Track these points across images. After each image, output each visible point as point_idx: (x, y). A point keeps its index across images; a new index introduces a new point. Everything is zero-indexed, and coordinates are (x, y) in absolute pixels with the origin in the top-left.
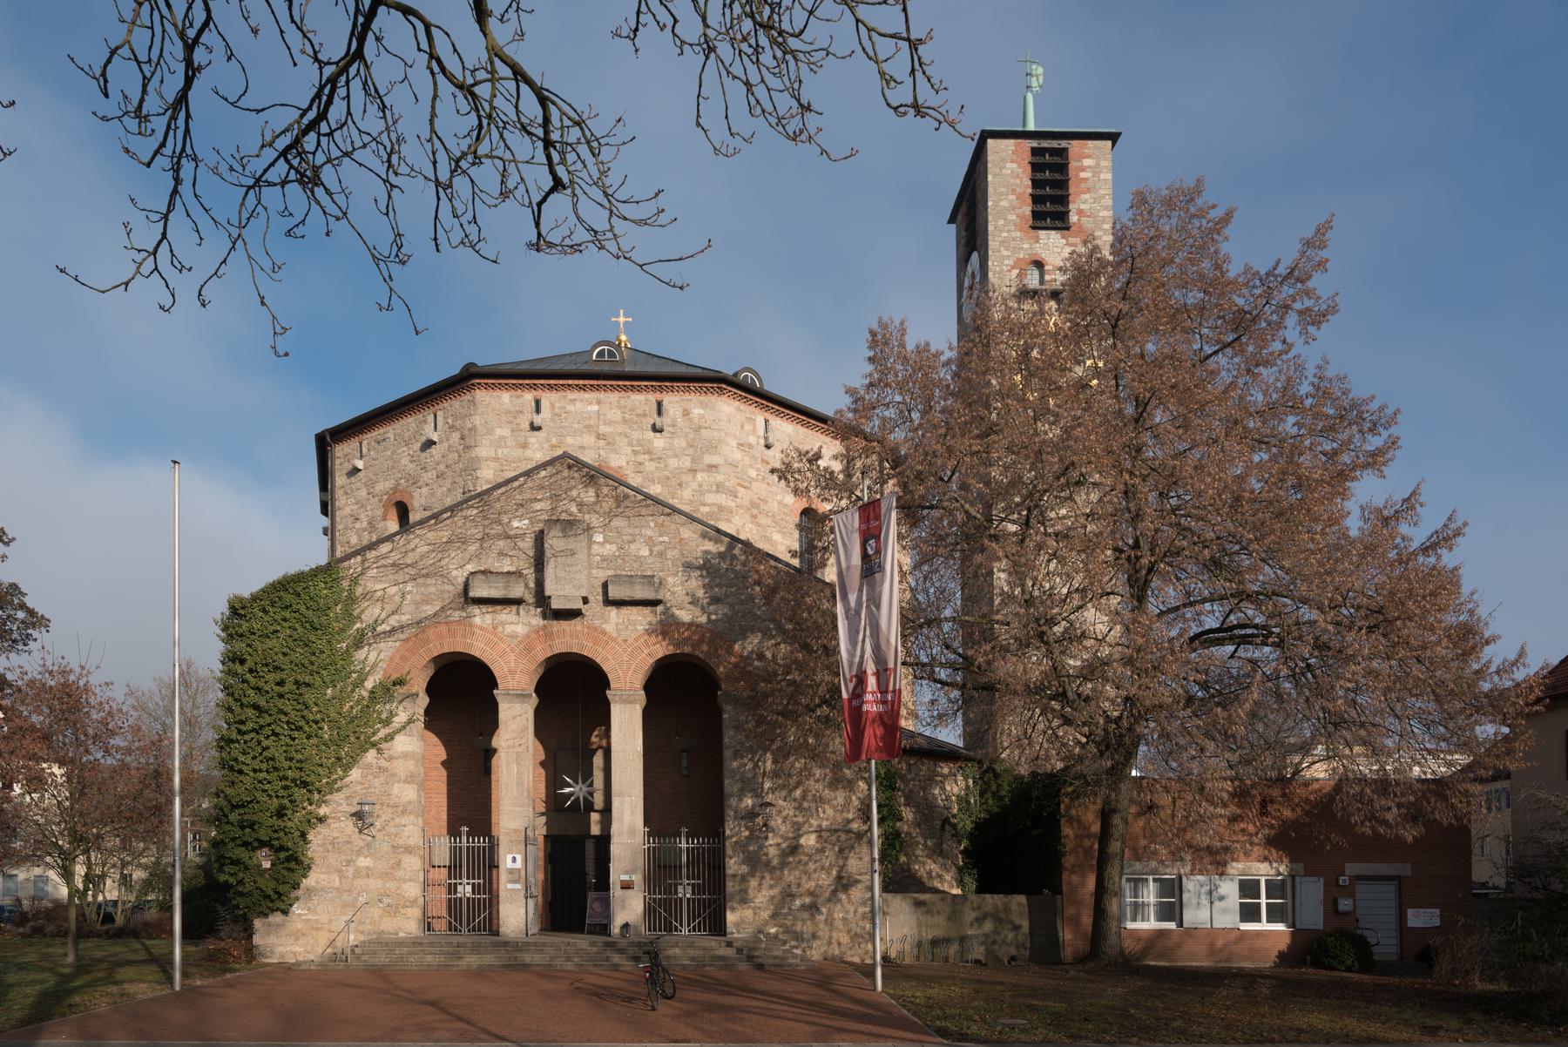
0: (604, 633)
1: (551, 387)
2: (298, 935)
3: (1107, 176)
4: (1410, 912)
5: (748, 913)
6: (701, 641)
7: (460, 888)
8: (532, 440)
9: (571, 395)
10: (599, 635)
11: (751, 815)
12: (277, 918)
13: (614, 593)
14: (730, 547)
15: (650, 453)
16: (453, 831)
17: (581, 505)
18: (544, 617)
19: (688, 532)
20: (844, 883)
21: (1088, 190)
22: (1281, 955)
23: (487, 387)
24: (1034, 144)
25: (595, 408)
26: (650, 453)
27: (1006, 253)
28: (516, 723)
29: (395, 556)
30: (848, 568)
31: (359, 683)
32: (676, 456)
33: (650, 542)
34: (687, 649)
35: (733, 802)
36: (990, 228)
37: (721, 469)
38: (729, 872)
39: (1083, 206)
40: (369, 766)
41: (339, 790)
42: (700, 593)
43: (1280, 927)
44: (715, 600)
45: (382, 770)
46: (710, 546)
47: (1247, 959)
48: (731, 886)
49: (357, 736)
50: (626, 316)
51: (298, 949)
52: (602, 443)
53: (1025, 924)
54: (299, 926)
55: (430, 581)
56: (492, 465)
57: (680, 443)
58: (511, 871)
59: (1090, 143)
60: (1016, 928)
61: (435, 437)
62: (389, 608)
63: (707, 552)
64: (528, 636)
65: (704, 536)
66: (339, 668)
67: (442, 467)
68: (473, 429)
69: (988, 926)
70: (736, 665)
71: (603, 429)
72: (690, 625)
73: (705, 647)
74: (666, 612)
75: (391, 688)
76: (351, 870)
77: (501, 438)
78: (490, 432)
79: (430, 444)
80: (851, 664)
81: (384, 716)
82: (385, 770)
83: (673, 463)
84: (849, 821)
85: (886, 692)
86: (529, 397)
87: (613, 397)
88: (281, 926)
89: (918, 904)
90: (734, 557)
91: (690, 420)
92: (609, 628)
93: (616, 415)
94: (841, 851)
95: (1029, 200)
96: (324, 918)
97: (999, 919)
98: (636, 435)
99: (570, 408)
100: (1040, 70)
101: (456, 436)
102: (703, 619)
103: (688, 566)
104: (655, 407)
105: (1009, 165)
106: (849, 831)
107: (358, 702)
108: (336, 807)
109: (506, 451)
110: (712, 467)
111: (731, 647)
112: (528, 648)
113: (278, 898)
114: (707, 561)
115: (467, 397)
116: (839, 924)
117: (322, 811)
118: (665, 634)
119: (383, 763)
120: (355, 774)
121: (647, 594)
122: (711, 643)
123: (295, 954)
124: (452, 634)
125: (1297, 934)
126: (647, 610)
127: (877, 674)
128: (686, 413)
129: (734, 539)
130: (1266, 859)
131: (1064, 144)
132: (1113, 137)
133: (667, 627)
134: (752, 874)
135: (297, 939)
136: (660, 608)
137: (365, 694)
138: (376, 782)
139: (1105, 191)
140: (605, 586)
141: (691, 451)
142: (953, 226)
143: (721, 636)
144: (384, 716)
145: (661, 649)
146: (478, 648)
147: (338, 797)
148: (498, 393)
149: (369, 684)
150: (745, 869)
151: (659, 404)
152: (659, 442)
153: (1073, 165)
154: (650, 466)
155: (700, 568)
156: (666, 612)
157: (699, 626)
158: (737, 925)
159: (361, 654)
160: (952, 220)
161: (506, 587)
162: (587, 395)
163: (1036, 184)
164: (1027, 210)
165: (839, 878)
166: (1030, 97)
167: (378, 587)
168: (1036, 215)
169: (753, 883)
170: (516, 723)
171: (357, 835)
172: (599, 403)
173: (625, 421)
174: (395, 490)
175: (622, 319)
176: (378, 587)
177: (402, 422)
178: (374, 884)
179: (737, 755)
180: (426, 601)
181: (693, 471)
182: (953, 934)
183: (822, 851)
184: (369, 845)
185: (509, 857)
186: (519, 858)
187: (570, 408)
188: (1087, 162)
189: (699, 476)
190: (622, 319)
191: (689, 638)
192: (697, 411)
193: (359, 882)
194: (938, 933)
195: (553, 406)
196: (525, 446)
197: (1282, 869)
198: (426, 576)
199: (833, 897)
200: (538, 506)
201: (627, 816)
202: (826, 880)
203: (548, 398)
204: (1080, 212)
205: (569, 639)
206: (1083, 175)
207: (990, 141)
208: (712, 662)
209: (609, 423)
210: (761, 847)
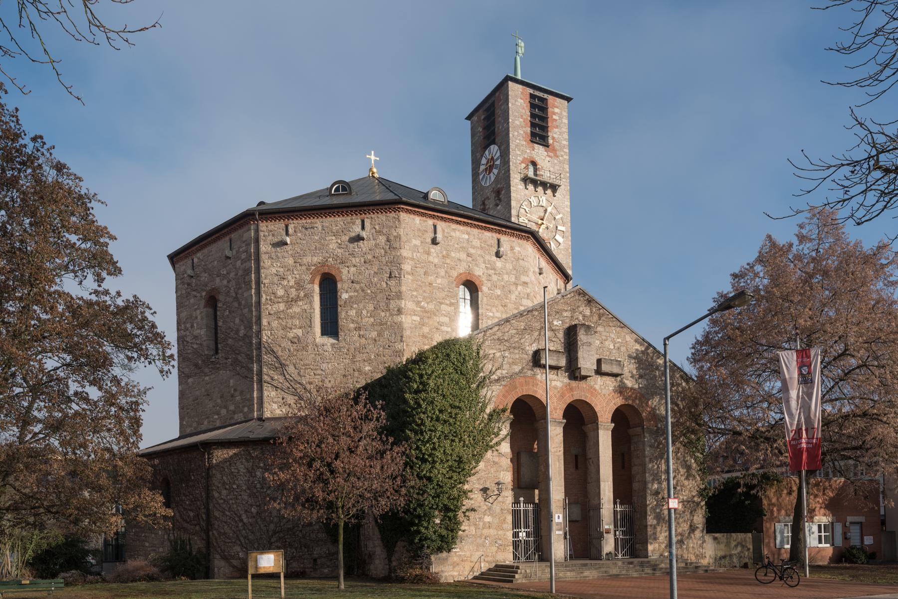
0: (595, 390)
1: (442, 219)
2: (455, 565)
3: (565, 121)
4: (865, 537)
5: (657, 545)
6: (636, 398)
7: (520, 534)
8: (433, 250)
9: (454, 226)
10: (592, 390)
11: (657, 493)
12: (444, 554)
13: (605, 368)
14: (647, 348)
15: (495, 270)
16: (615, 503)
17: (584, 316)
18: (570, 378)
19: (629, 338)
20: (692, 529)
21: (557, 127)
22: (830, 559)
23: (407, 211)
24: (531, 91)
25: (466, 237)
26: (495, 270)
27: (519, 153)
28: (556, 436)
29: (499, 334)
30: (791, 378)
31: (482, 410)
32: (507, 273)
33: (613, 341)
34: (630, 402)
35: (650, 485)
36: (511, 135)
37: (530, 285)
38: (649, 523)
39: (555, 136)
40: (489, 460)
41: (474, 475)
42: (635, 372)
43: (828, 545)
44: (641, 377)
45: (495, 463)
46: (638, 347)
47: (821, 560)
48: (650, 531)
49: (482, 443)
50: (375, 155)
51: (456, 574)
52: (469, 259)
53: (751, 547)
54: (455, 559)
55: (516, 351)
56: (411, 262)
57: (509, 266)
58: (558, 524)
59: (558, 100)
60: (749, 549)
61: (364, 234)
62: (497, 365)
63: (637, 350)
64: (562, 388)
65: (636, 341)
66: (474, 402)
67: (370, 257)
68: (398, 237)
69: (739, 549)
70: (650, 412)
71: (472, 251)
72: (632, 389)
73: (637, 402)
74: (621, 381)
75: (495, 415)
76: (481, 524)
77: (415, 246)
78: (409, 241)
79: (359, 238)
80: (791, 424)
81: (496, 430)
82: (497, 463)
83: (506, 277)
84: (694, 497)
85: (813, 438)
86: (430, 222)
87: (475, 231)
88: (446, 559)
89: (715, 539)
90: (648, 354)
91: (514, 253)
92: (597, 387)
93: (477, 243)
94: (691, 512)
95: (529, 124)
96: (468, 554)
97: (741, 544)
98: (487, 257)
99: (453, 234)
100: (523, 44)
101: (382, 239)
102: (636, 386)
103: (630, 357)
104: (496, 242)
105: (519, 100)
106: (694, 502)
107: (482, 421)
108: (473, 484)
109: (418, 255)
110: (525, 283)
111: (647, 402)
112: (563, 396)
113: (446, 543)
114: (637, 355)
115: (393, 214)
116: (691, 549)
117: (466, 487)
118: (621, 393)
119: (496, 459)
120: (482, 465)
121: (616, 370)
122: (640, 400)
123: (453, 576)
124: (527, 383)
125: (835, 548)
126: (613, 379)
127: (807, 430)
128: (512, 249)
129: (650, 345)
130: (825, 515)
131: (546, 96)
132: (569, 99)
133: (621, 390)
134: (658, 524)
135: (454, 567)
136: (619, 379)
137: (486, 416)
138: (492, 470)
139: (565, 129)
140: (599, 361)
141: (514, 272)
142: (469, 122)
143: (644, 395)
144: (496, 430)
145: (619, 401)
146: (540, 394)
147: (473, 479)
148: (412, 216)
149: (488, 411)
150: (655, 522)
151: (499, 240)
152: (499, 263)
153: (550, 110)
154: (495, 278)
155: (635, 358)
156: (621, 381)
157: (635, 390)
158: (653, 551)
159: (483, 392)
160: (469, 118)
161: (558, 360)
162: (461, 228)
163: (533, 116)
164: (529, 130)
165: (691, 526)
166: (518, 59)
167: (491, 352)
168: (533, 135)
169: (659, 529)
170: (556, 436)
171: (483, 503)
172: (468, 234)
173: (482, 248)
174: (323, 264)
175: (373, 157)
176: (491, 352)
177: (329, 219)
178: (492, 532)
179: (651, 461)
180: (514, 363)
181: (516, 284)
182: (728, 553)
183: (684, 512)
184: (489, 509)
185: (557, 516)
186: (561, 516)
187: (453, 234)
188: (556, 110)
189: (520, 288)
190: (373, 157)
191: (630, 396)
192: (517, 249)
193: (486, 532)
194: (720, 554)
195: (443, 231)
196: (428, 253)
197: (830, 519)
198: (514, 348)
199: (689, 537)
200: (565, 314)
201: (607, 493)
202: (685, 527)
203: (441, 225)
204: (553, 138)
205: (580, 392)
206: (554, 117)
207: (510, 82)
208: (640, 410)
209: (474, 247)
210: (661, 510)
